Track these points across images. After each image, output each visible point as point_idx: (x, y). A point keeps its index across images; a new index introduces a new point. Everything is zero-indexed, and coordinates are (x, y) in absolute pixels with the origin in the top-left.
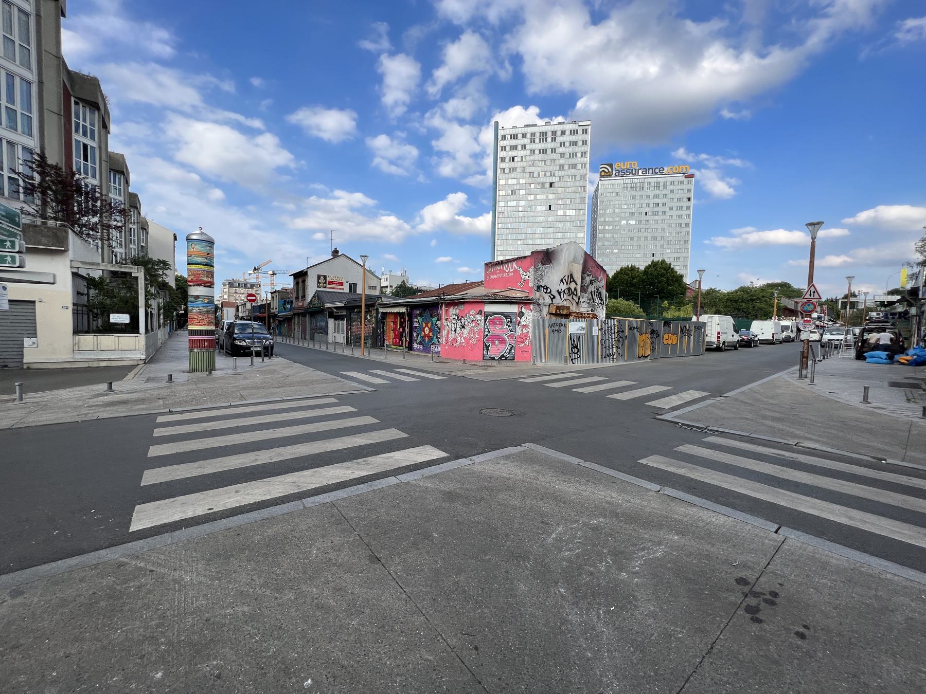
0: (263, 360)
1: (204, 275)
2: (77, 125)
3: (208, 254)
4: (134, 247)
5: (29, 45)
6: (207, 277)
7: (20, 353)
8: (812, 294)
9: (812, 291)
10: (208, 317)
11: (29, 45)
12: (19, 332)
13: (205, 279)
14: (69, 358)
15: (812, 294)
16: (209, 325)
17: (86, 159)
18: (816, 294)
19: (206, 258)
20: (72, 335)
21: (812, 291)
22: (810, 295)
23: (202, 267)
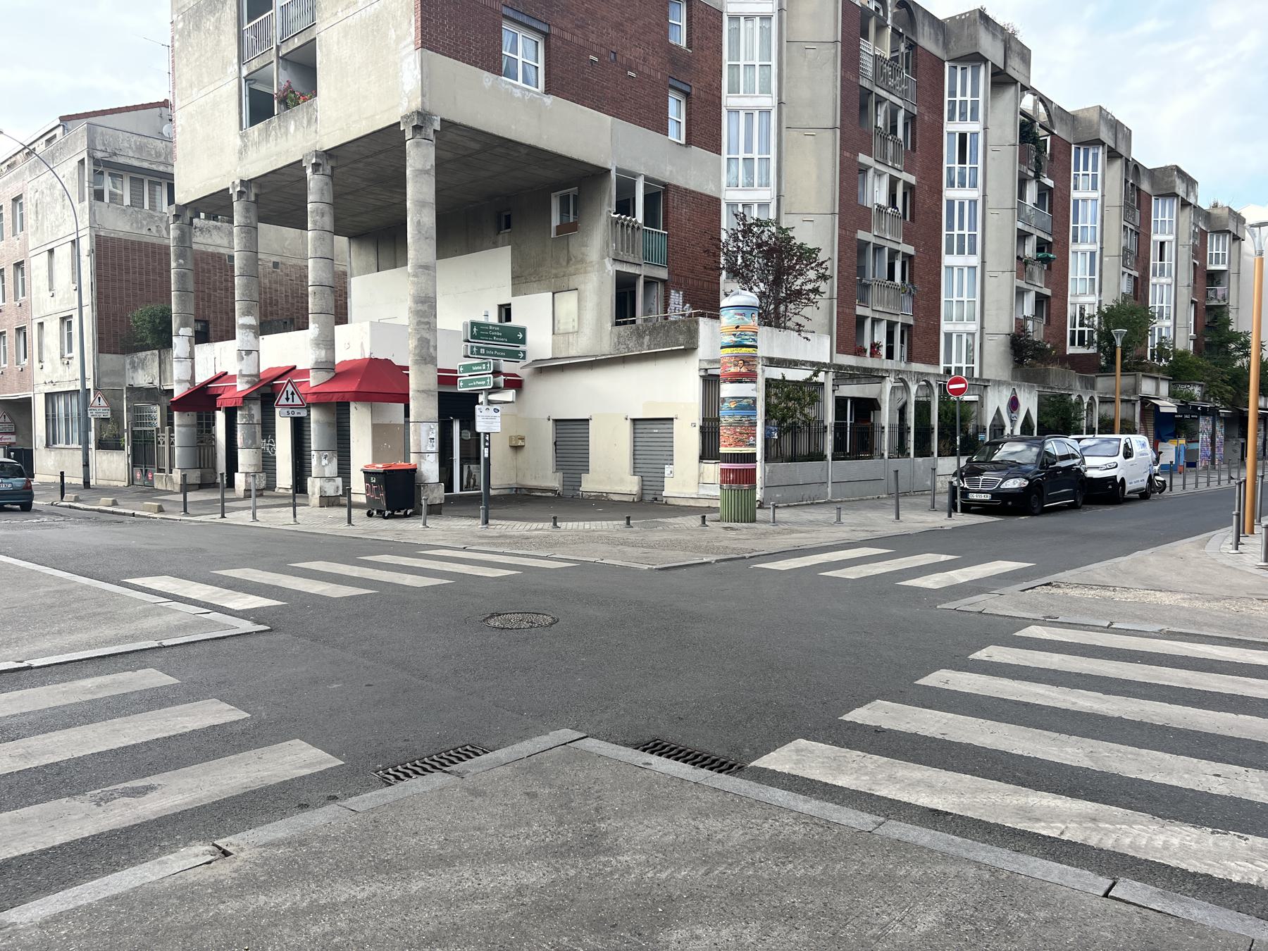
0: (424, 524)
1: (731, 363)
2: (953, 103)
3: (737, 327)
4: (1169, 280)
5: (537, 62)
6: (735, 365)
7: (661, 484)
8: (290, 396)
9: (290, 393)
10: (735, 433)
11: (537, 62)
12: (665, 457)
13: (733, 370)
14: (693, 493)
15: (290, 396)
16: (736, 446)
17: (962, 160)
18: (296, 396)
19: (734, 335)
20: (697, 461)
21: (290, 393)
22: (287, 399)
23: (729, 350)
